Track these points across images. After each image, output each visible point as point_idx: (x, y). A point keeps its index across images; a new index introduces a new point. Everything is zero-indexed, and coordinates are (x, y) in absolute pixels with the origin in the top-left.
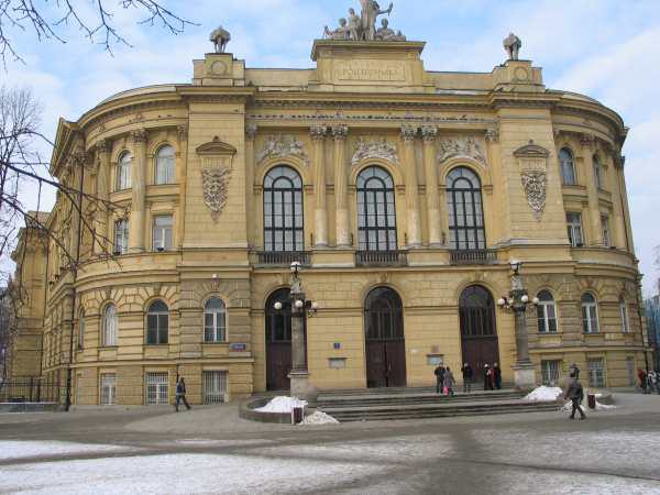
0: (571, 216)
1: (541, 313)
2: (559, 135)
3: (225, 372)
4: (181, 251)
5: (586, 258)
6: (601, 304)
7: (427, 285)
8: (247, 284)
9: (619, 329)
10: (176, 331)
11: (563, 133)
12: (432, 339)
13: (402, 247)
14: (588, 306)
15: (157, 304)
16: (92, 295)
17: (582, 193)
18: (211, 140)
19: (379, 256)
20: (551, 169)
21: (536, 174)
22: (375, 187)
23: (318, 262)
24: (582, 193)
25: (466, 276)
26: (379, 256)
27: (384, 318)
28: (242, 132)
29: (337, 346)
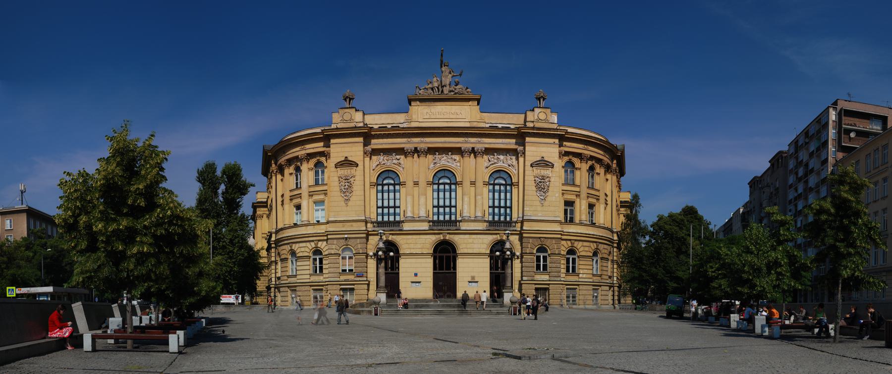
0: (569, 204)
1: (568, 262)
2: (563, 154)
3: (353, 289)
4: (328, 223)
5: (572, 229)
6: (578, 257)
7: (470, 241)
8: (365, 240)
9: (590, 272)
10: (327, 266)
11: (567, 154)
12: (473, 275)
13: (459, 218)
14: (571, 257)
15: (317, 252)
16: (284, 247)
17: (577, 189)
18: (343, 159)
19: (445, 223)
20: (556, 175)
21: (543, 178)
22: (445, 179)
23: (407, 227)
24: (577, 189)
25: (495, 236)
26: (445, 223)
27: (445, 258)
28: (362, 153)
29: (416, 275)
